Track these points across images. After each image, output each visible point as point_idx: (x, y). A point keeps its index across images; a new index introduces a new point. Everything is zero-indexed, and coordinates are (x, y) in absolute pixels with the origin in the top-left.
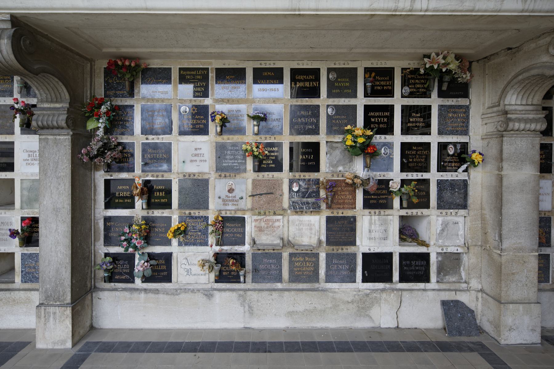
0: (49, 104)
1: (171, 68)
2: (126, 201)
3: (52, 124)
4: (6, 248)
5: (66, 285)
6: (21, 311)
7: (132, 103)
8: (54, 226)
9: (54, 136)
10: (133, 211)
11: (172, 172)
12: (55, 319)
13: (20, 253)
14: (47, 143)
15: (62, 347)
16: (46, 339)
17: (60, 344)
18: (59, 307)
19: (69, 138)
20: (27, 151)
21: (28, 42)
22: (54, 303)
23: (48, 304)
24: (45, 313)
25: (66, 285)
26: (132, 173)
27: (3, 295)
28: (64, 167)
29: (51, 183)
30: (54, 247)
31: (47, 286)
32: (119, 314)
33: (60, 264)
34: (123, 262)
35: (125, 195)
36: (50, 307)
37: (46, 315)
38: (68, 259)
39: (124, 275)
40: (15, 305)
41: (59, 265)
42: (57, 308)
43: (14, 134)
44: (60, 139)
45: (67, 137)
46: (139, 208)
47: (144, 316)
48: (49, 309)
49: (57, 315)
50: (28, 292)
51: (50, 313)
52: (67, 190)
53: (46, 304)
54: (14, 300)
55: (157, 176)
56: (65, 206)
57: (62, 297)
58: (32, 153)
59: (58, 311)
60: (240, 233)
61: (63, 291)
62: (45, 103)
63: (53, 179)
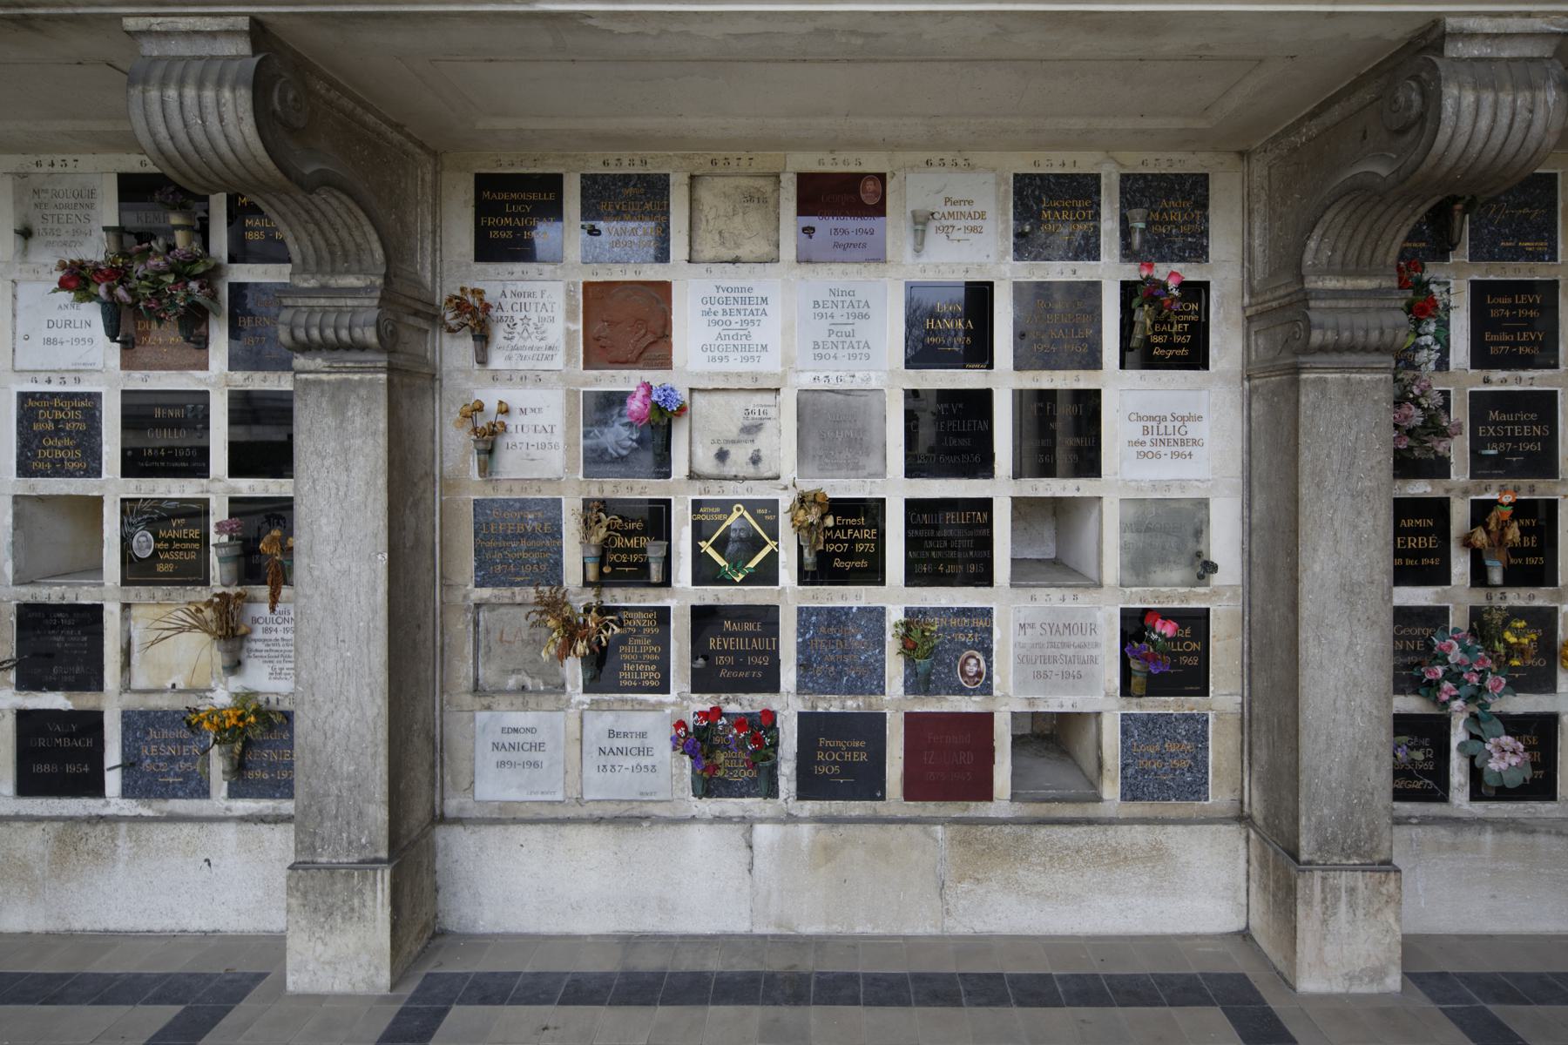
0: (1341, 278)
1: (1556, 175)
2: (1424, 561)
3: (352, 339)
4: (1077, 698)
5: (1380, 806)
6: (1135, 884)
7: (1444, 275)
8: (1342, 635)
9: (1344, 372)
10: (1445, 591)
11: (1560, 477)
12: (1352, 906)
13: (1119, 713)
14: (1323, 393)
15: (1374, 989)
16: (1326, 964)
17: (1367, 980)
18: (1363, 871)
19: (1386, 378)
20: (1140, 418)
21: (290, 96)
22: (1344, 862)
23: (1325, 864)
24: (1323, 891)
25: (1380, 806)
26: (1444, 482)
27: (1084, 836)
28: (1374, 462)
29: (1335, 511)
30: (1344, 696)
31: (1321, 810)
32: (1420, 892)
33: (1360, 748)
34: (1416, 739)
35: (1423, 544)
36: (1338, 873)
37: (1329, 896)
38: (1384, 732)
39: (1419, 780)
40: (1118, 867)
41: (1357, 749)
42: (1359, 874)
43: (1101, 369)
44: (1362, 380)
45: (1383, 376)
46: (1461, 582)
47: (1494, 897)
48: (1335, 878)
49: (1360, 896)
50: (1158, 829)
51: (1339, 889)
52: (1381, 531)
53: (1321, 862)
54: (1115, 852)
55: (1516, 490)
56: (1377, 577)
57: (1365, 843)
58: (1155, 424)
59: (1361, 885)
60: (762, 653)
61: (1368, 825)
62: (1328, 277)
63: (1342, 497)
